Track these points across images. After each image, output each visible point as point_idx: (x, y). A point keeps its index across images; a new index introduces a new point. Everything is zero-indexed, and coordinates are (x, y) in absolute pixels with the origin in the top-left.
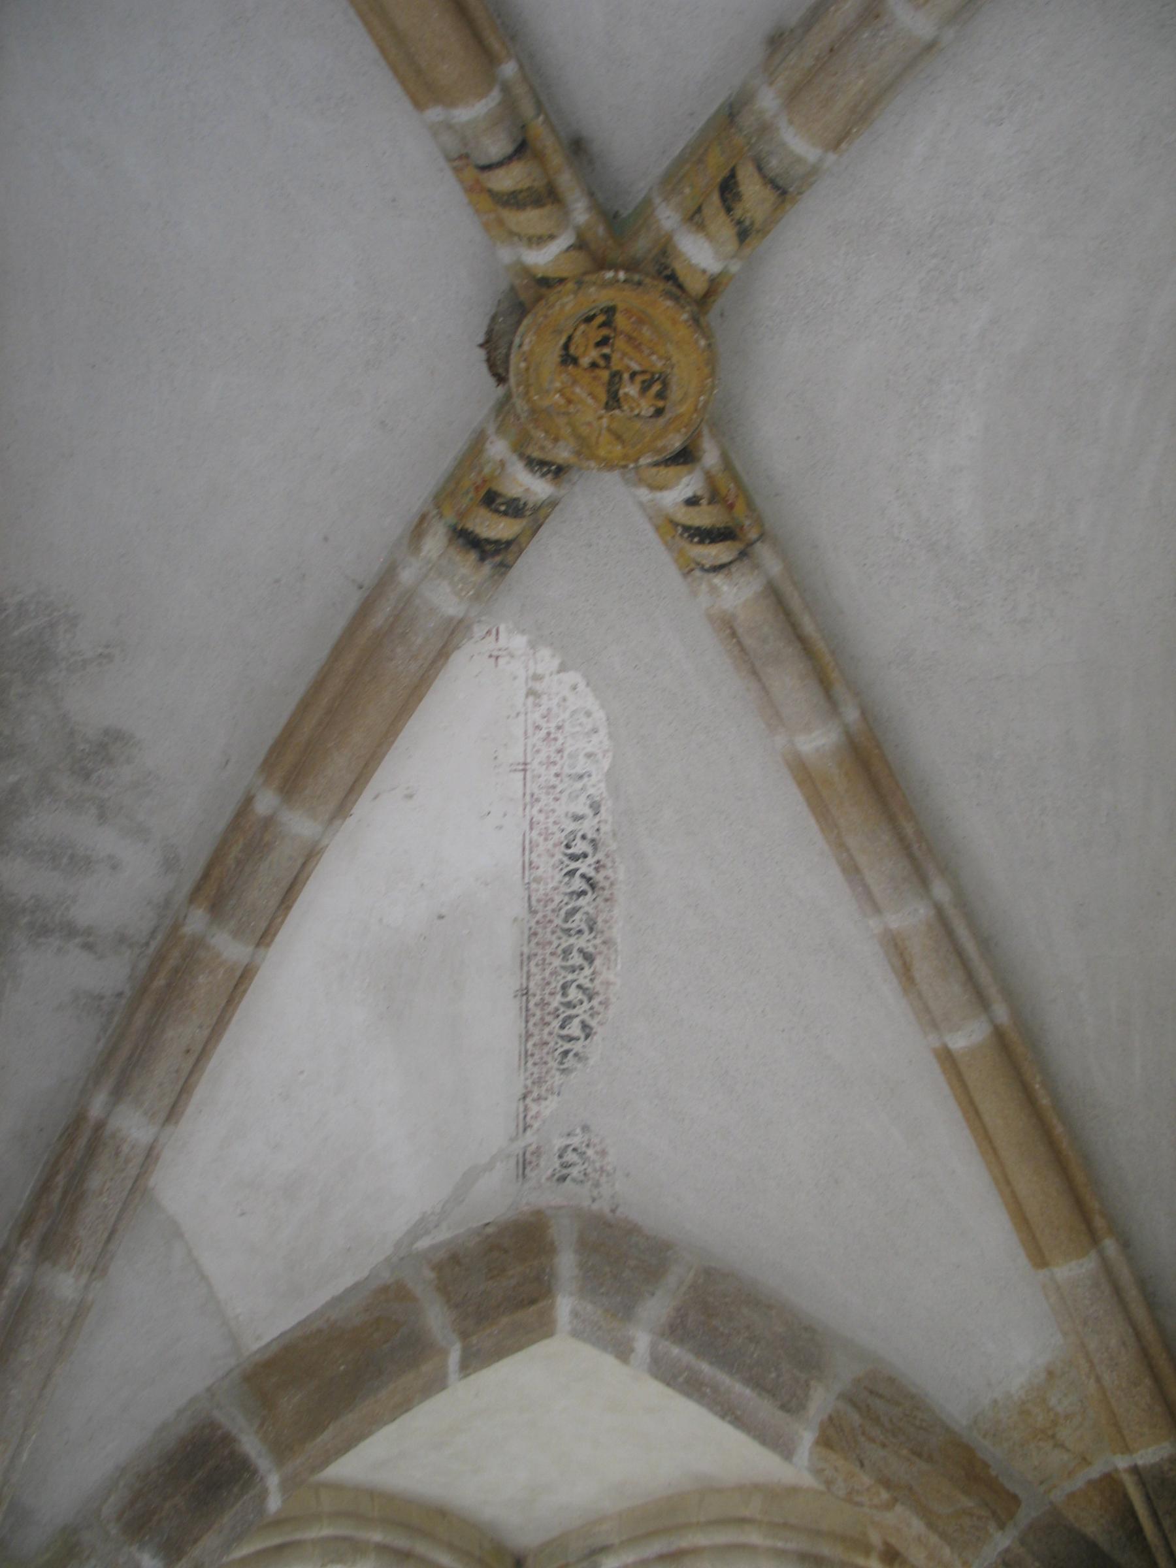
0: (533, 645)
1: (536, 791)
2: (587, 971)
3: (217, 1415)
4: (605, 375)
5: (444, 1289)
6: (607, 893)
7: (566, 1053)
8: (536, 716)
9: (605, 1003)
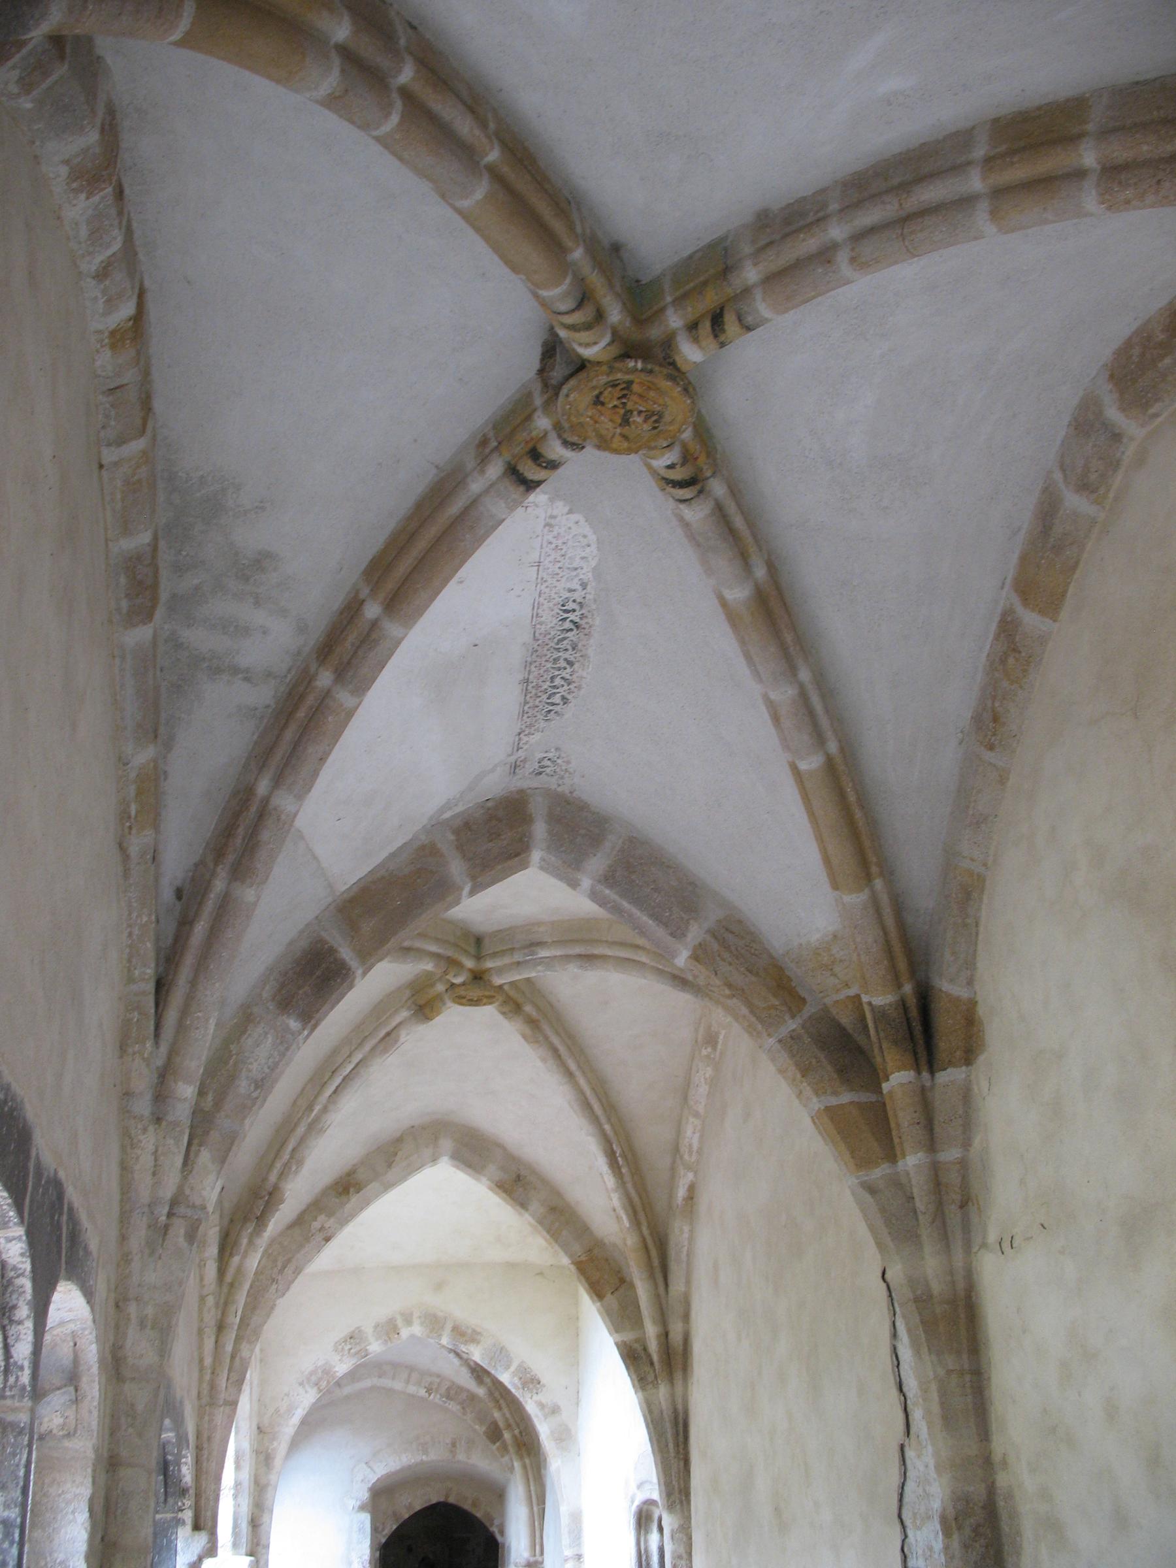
0: (552, 500)
1: (545, 576)
2: (569, 670)
3: (323, 934)
4: (622, 411)
5: (460, 847)
6: (586, 631)
7: (550, 711)
8: (550, 537)
9: (579, 688)
